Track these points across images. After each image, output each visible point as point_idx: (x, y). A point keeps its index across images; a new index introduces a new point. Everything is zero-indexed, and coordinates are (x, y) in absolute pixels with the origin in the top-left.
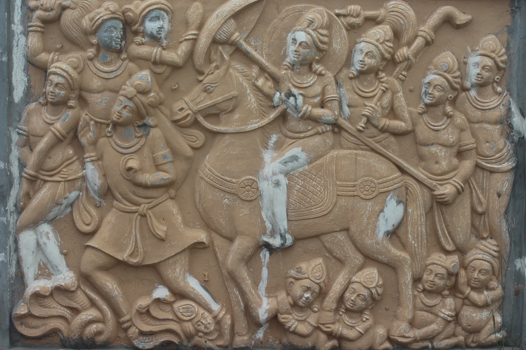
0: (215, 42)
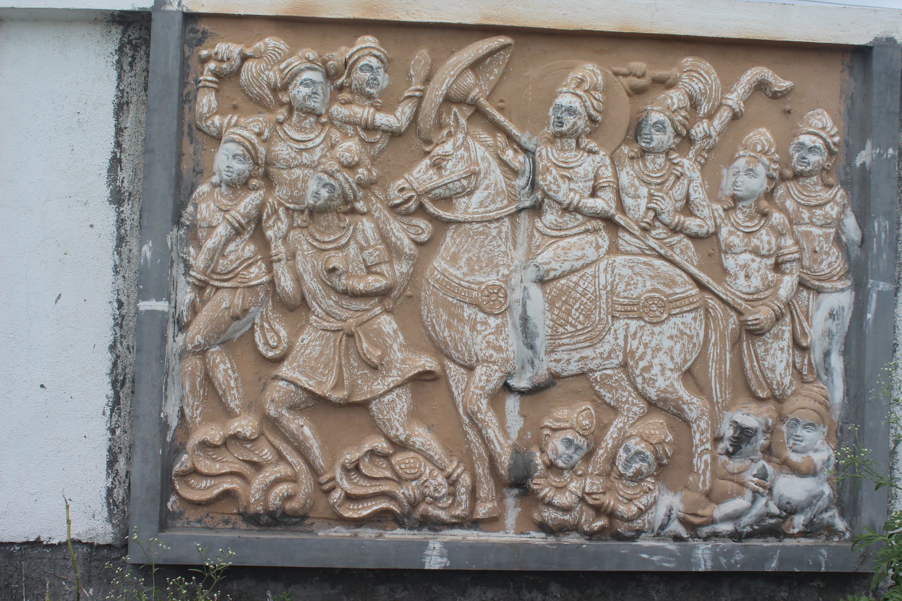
0: (448, 100)
